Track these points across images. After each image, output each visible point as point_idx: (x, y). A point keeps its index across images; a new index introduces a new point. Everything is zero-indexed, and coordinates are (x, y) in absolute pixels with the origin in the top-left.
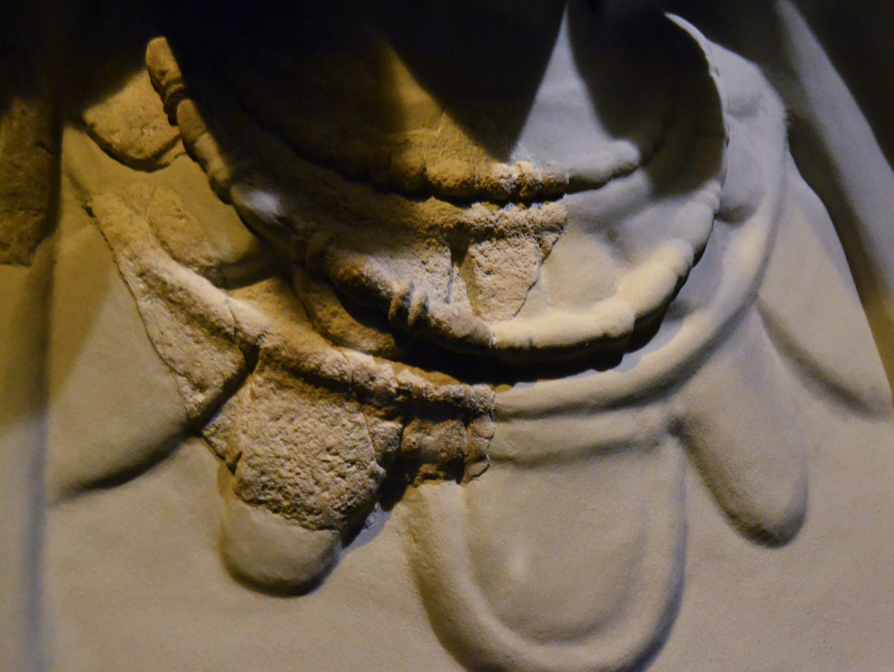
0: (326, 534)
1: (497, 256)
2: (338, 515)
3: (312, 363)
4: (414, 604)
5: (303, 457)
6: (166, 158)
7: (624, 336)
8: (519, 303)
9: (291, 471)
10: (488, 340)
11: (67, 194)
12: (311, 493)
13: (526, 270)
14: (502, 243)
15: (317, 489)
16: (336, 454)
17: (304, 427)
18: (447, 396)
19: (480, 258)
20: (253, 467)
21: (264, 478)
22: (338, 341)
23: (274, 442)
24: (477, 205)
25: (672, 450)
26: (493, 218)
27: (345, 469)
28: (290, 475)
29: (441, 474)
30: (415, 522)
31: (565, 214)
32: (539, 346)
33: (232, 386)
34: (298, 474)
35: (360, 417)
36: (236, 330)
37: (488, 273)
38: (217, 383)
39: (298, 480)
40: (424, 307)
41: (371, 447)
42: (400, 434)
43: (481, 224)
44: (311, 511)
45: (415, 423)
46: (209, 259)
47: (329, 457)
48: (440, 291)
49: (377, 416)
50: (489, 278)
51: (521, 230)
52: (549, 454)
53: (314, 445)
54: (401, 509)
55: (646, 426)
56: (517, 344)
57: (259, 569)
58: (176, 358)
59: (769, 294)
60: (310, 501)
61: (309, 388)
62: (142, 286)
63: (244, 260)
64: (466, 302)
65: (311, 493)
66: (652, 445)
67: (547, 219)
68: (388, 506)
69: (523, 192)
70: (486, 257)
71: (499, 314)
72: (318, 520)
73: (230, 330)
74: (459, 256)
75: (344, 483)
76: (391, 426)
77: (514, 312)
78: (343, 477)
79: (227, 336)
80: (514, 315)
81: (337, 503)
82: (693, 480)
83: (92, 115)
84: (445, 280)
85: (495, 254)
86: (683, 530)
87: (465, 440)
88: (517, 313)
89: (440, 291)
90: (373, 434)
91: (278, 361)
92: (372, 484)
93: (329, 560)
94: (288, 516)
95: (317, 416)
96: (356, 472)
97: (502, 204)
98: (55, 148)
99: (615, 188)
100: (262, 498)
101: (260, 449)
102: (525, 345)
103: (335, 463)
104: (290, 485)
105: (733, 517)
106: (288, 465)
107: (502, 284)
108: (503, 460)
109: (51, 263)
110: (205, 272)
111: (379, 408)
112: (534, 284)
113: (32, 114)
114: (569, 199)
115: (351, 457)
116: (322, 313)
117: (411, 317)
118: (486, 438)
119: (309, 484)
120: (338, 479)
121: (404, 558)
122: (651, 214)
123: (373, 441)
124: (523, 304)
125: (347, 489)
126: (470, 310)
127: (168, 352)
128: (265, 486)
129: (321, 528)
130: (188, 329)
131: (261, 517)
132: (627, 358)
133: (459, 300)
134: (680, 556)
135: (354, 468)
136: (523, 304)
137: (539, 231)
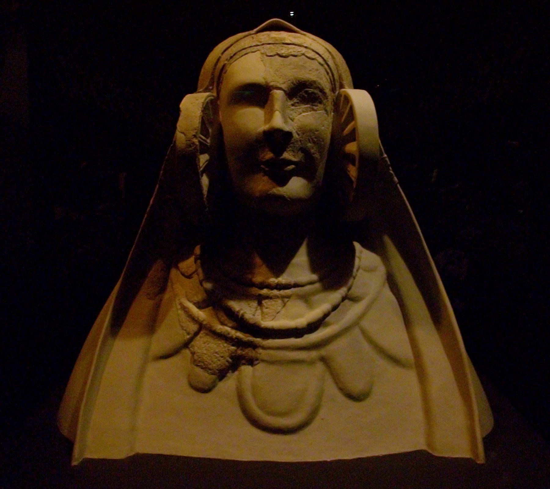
0: (214, 376)
2: (217, 371)
3: (214, 329)
4: (236, 399)
6: (193, 275)
7: (303, 329)
8: (273, 317)
11: (169, 284)
12: (210, 364)
14: (271, 300)
15: (212, 363)
16: (218, 354)
21: (199, 359)
22: (223, 324)
24: (265, 290)
29: (247, 363)
31: (291, 293)
32: (276, 329)
33: (196, 334)
35: (225, 345)
38: (192, 333)
39: (207, 360)
44: (210, 369)
45: (240, 348)
46: (195, 300)
47: (216, 355)
48: (252, 312)
49: (230, 345)
50: (267, 310)
51: (277, 297)
54: (236, 373)
57: (200, 386)
58: (184, 326)
59: (365, 324)
60: (210, 366)
62: (179, 307)
64: (260, 316)
65: (210, 364)
66: (312, 363)
68: (233, 371)
71: (267, 320)
73: (196, 319)
74: (260, 304)
76: (233, 348)
77: (272, 319)
78: (219, 360)
79: (196, 321)
80: (273, 320)
82: (328, 376)
83: (181, 265)
85: (269, 303)
89: (252, 312)
90: (228, 350)
92: (227, 364)
98: (168, 272)
99: (308, 288)
100: (199, 364)
101: (199, 351)
105: (341, 389)
106: (206, 356)
108: (263, 361)
109: (161, 300)
110: (195, 304)
111: (231, 343)
114: (293, 290)
115: (222, 355)
117: (239, 317)
119: (210, 362)
120: (218, 361)
122: (322, 295)
124: (395, 360)
126: (261, 318)
127: (183, 325)
128: (199, 362)
129: (212, 374)
130: (188, 319)
131: (198, 370)
132: (306, 336)
133: (258, 315)
134: (320, 397)
135: (222, 359)
136: (395, 360)
137: (283, 297)
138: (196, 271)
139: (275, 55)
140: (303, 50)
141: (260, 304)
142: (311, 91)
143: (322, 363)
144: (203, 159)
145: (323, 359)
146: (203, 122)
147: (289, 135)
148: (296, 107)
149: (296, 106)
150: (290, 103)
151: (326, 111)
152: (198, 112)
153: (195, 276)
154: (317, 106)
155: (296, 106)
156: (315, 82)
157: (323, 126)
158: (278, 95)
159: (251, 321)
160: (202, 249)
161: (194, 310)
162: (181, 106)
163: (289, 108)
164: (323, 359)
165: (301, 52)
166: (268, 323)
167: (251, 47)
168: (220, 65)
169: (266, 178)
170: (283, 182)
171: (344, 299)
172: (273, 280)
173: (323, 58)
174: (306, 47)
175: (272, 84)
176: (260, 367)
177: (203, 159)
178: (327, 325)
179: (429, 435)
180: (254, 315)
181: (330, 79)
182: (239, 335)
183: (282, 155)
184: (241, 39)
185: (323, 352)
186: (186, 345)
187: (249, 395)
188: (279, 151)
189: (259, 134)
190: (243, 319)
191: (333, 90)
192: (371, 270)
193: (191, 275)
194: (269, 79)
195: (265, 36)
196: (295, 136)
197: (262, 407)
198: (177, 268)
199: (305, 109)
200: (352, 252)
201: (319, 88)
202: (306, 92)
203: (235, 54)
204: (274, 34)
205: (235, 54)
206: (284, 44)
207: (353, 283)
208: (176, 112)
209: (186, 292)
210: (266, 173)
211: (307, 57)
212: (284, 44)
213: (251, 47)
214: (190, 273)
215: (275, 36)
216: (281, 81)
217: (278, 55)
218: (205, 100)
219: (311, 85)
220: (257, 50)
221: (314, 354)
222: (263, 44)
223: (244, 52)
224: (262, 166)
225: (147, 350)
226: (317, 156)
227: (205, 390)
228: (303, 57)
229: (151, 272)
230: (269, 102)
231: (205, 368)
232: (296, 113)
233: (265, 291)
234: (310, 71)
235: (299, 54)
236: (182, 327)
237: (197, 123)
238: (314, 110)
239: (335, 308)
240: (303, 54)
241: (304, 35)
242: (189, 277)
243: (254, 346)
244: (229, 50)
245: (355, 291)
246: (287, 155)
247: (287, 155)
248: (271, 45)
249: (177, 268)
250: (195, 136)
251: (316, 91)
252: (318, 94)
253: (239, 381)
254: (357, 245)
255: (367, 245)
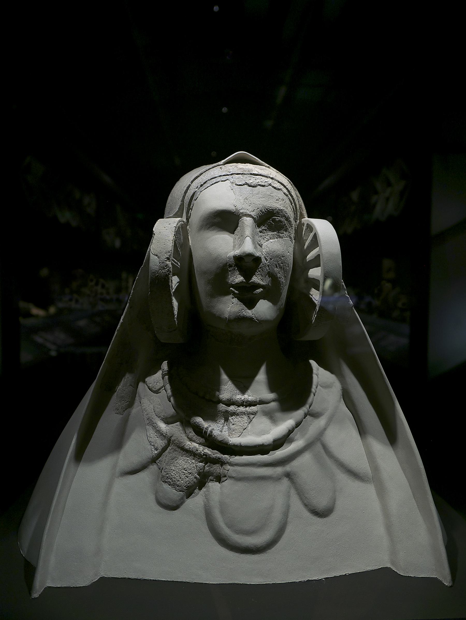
1: (236, 420)
4: (204, 517)
5: (177, 470)
6: (161, 391)
7: (269, 445)
9: (174, 474)
10: (228, 442)
11: (137, 398)
13: (243, 424)
15: (180, 480)
17: (179, 462)
18: (216, 457)
19: (231, 420)
20: (165, 472)
22: (191, 440)
23: (171, 465)
25: (285, 481)
26: (236, 410)
27: (188, 475)
28: (174, 475)
29: (215, 480)
30: (206, 493)
34: (176, 475)
36: (166, 434)
37: (233, 425)
38: (160, 448)
40: (211, 432)
41: (196, 469)
42: (204, 467)
43: (232, 411)
51: (243, 413)
52: (245, 477)
53: (181, 467)
54: (204, 489)
55: (276, 473)
56: (236, 444)
57: (164, 501)
60: (178, 483)
61: (182, 452)
63: (172, 417)
65: (179, 481)
66: (277, 479)
67: (251, 411)
68: (200, 489)
69: (245, 403)
70: (233, 420)
71: (234, 436)
72: (179, 489)
74: (227, 420)
75: (187, 479)
81: (185, 484)
83: (148, 379)
84: (221, 426)
85: (236, 420)
86: (288, 508)
87: (221, 471)
88: (239, 436)
90: (196, 466)
91: (175, 444)
93: (182, 501)
94: (172, 487)
95: (183, 459)
96: (191, 476)
97: (239, 406)
102: (238, 444)
103: (185, 473)
104: (173, 478)
105: (306, 505)
107: (236, 428)
108: (231, 477)
112: (245, 429)
113: (130, 378)
116: (188, 432)
118: (227, 471)
119: (178, 478)
121: (203, 503)
123: (196, 468)
124: (241, 434)
125: (188, 481)
127: (150, 439)
129: (180, 491)
131: (166, 486)
133: (225, 432)
134: (286, 514)
137: (249, 414)
138: (164, 386)
139: (244, 184)
140: (270, 181)
141: (227, 420)
142: (278, 219)
143: (287, 479)
144: (175, 280)
145: (288, 475)
146: (175, 246)
147: (257, 260)
148: (264, 234)
149: (263, 232)
150: (258, 230)
151: (291, 238)
152: (171, 237)
153: (163, 391)
154: (283, 233)
155: (265, 233)
156: (282, 210)
157: (289, 252)
158: (248, 222)
159: (220, 438)
160: (169, 365)
161: (163, 426)
162: (154, 229)
163: (258, 235)
164: (288, 475)
165: (268, 183)
166: (234, 440)
167: (220, 176)
168: (190, 193)
169: (235, 300)
170: (251, 304)
171: (306, 415)
172: (239, 397)
173: (287, 189)
174: (272, 178)
175: (241, 211)
176: (227, 483)
177: (175, 280)
178: (291, 441)
179: (393, 553)
180: (221, 431)
181: (293, 209)
182: (208, 451)
183: (251, 278)
184: (210, 169)
185: (288, 468)
186: (154, 460)
187: (217, 513)
188: (248, 274)
189: (229, 258)
190: (212, 435)
191: (295, 219)
192: (327, 386)
193: (160, 389)
194: (239, 206)
195: (233, 167)
196: (263, 260)
197: (230, 526)
198: (144, 382)
199: (272, 236)
200: (310, 370)
201: (285, 216)
202: (274, 220)
203: (205, 183)
204: (240, 166)
205: (205, 183)
206: (251, 174)
207: (313, 399)
208: (150, 234)
209: (154, 407)
210: (235, 296)
211: (273, 187)
212: (251, 174)
213: (220, 176)
214: (158, 388)
215: (243, 167)
216: (251, 209)
217: (246, 184)
218: (177, 224)
219: (278, 213)
220: (226, 179)
221: (279, 470)
222: (232, 174)
223: (214, 181)
224: (231, 288)
225: (114, 466)
226: (283, 280)
227: (174, 508)
228: (271, 187)
229: (120, 387)
230: (239, 228)
231: (173, 485)
232: (264, 239)
233: (232, 408)
234: (277, 200)
235: (266, 184)
236: (150, 442)
237: (170, 245)
238: (280, 237)
239: (298, 424)
240: (270, 185)
241: (268, 167)
242: (157, 392)
243: (222, 463)
244: (199, 178)
245: (316, 407)
246: (256, 279)
247: (256, 279)
248: (240, 175)
249: (144, 382)
250: (168, 259)
251: (283, 219)
252: (284, 222)
253: (207, 498)
254: (313, 363)
255: (323, 364)
